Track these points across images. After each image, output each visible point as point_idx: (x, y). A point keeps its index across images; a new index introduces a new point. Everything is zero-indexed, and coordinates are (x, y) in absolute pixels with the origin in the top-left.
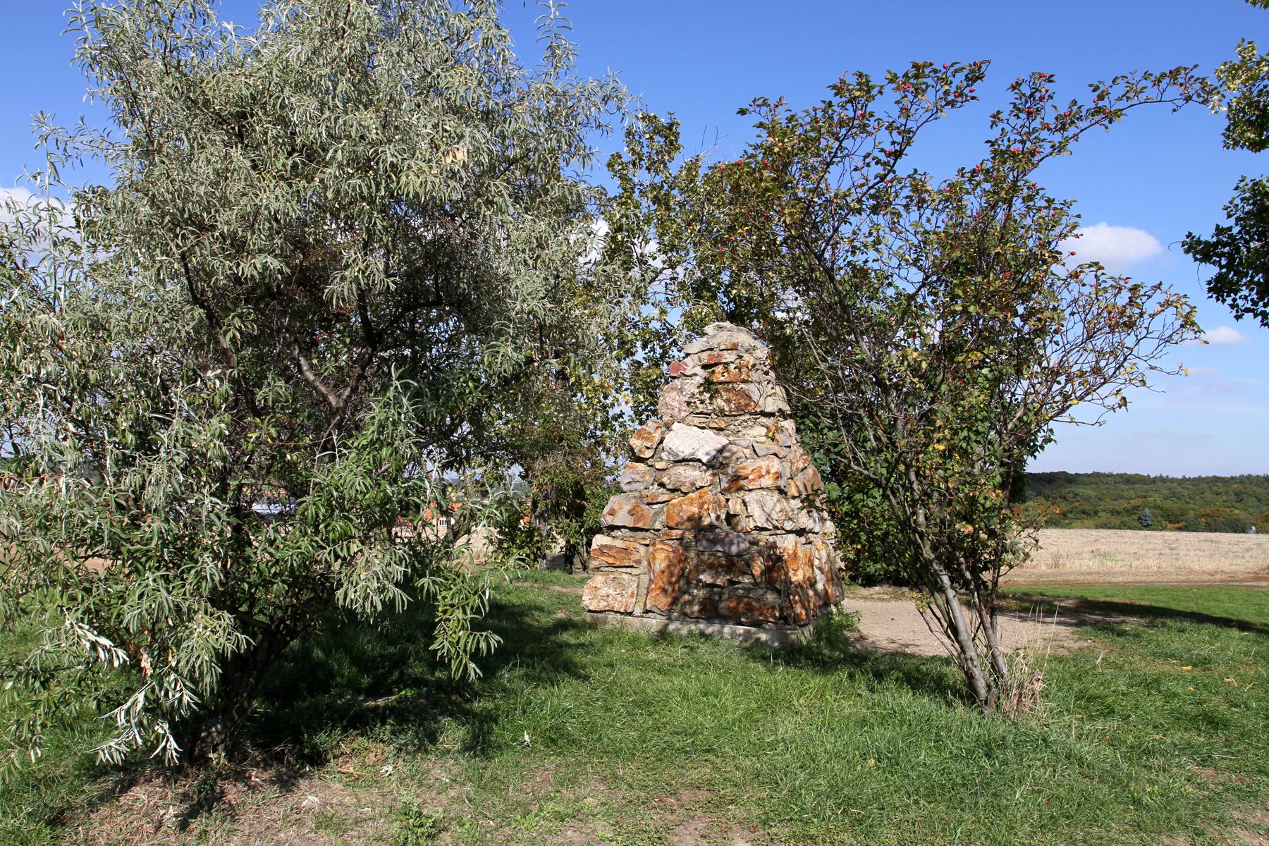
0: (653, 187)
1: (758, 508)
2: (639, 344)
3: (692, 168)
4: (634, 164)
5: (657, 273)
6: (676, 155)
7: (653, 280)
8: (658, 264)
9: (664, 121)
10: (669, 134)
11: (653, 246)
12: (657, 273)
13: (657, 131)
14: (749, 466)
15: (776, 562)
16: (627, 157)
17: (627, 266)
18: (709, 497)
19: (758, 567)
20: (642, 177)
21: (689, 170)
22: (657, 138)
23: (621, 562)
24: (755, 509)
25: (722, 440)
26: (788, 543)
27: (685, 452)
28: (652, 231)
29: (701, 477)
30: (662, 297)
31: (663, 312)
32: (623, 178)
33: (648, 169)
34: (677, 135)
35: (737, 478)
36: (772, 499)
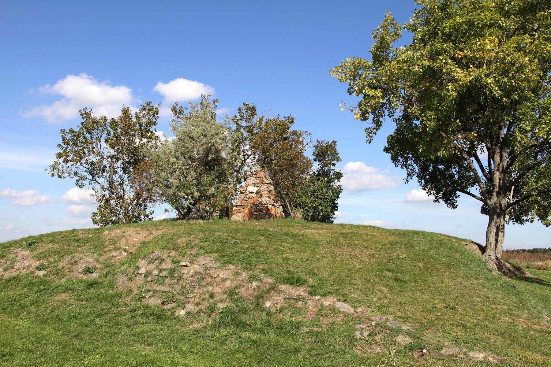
0: (247, 127)
1: (265, 200)
2: (243, 180)
3: (261, 120)
4: (241, 120)
5: (249, 156)
6: (255, 117)
7: (248, 158)
8: (249, 153)
9: (251, 106)
10: (253, 111)
11: (247, 147)
12: (249, 156)
13: (248, 109)
14: (263, 193)
15: (268, 209)
16: (239, 117)
17: (239, 154)
18: (255, 199)
19: (264, 211)
20: (244, 124)
21: (259, 121)
22: (249, 111)
23: (238, 212)
24: (264, 200)
25: (258, 188)
26: (270, 206)
27: (251, 191)
28: (247, 143)
29: (254, 195)
30: (251, 164)
31: (251, 169)
32: (238, 124)
33: (246, 121)
34: (255, 110)
35: (261, 195)
36: (267, 199)
